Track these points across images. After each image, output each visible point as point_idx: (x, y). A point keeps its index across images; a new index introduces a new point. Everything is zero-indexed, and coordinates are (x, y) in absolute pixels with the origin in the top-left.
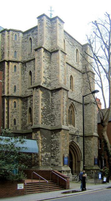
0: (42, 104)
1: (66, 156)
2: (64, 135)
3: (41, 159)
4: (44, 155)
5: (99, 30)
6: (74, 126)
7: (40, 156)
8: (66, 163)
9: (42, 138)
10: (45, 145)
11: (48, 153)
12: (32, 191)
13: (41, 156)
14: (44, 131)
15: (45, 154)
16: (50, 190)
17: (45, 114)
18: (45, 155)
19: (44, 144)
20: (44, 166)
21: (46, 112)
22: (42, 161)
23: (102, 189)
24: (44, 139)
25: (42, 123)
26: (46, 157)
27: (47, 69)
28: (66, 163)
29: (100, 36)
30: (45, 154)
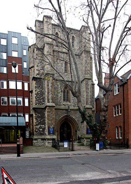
0: (35, 90)
1: (51, 127)
2: (50, 110)
3: (36, 130)
4: (38, 127)
5: (114, 5)
6: (70, 103)
7: (35, 127)
8: (51, 132)
9: (36, 115)
10: (39, 120)
11: (42, 126)
12: (2, 153)
13: (36, 128)
14: (38, 110)
15: (39, 126)
16: (51, 151)
17: (39, 97)
18: (39, 127)
19: (38, 119)
20: (38, 135)
21: (39, 95)
22: (36, 132)
23: (38, 157)
24: (38, 116)
25: (36, 104)
26: (41, 129)
27: (40, 63)
28: (51, 132)
29: (53, 8)
30: (39, 126)
